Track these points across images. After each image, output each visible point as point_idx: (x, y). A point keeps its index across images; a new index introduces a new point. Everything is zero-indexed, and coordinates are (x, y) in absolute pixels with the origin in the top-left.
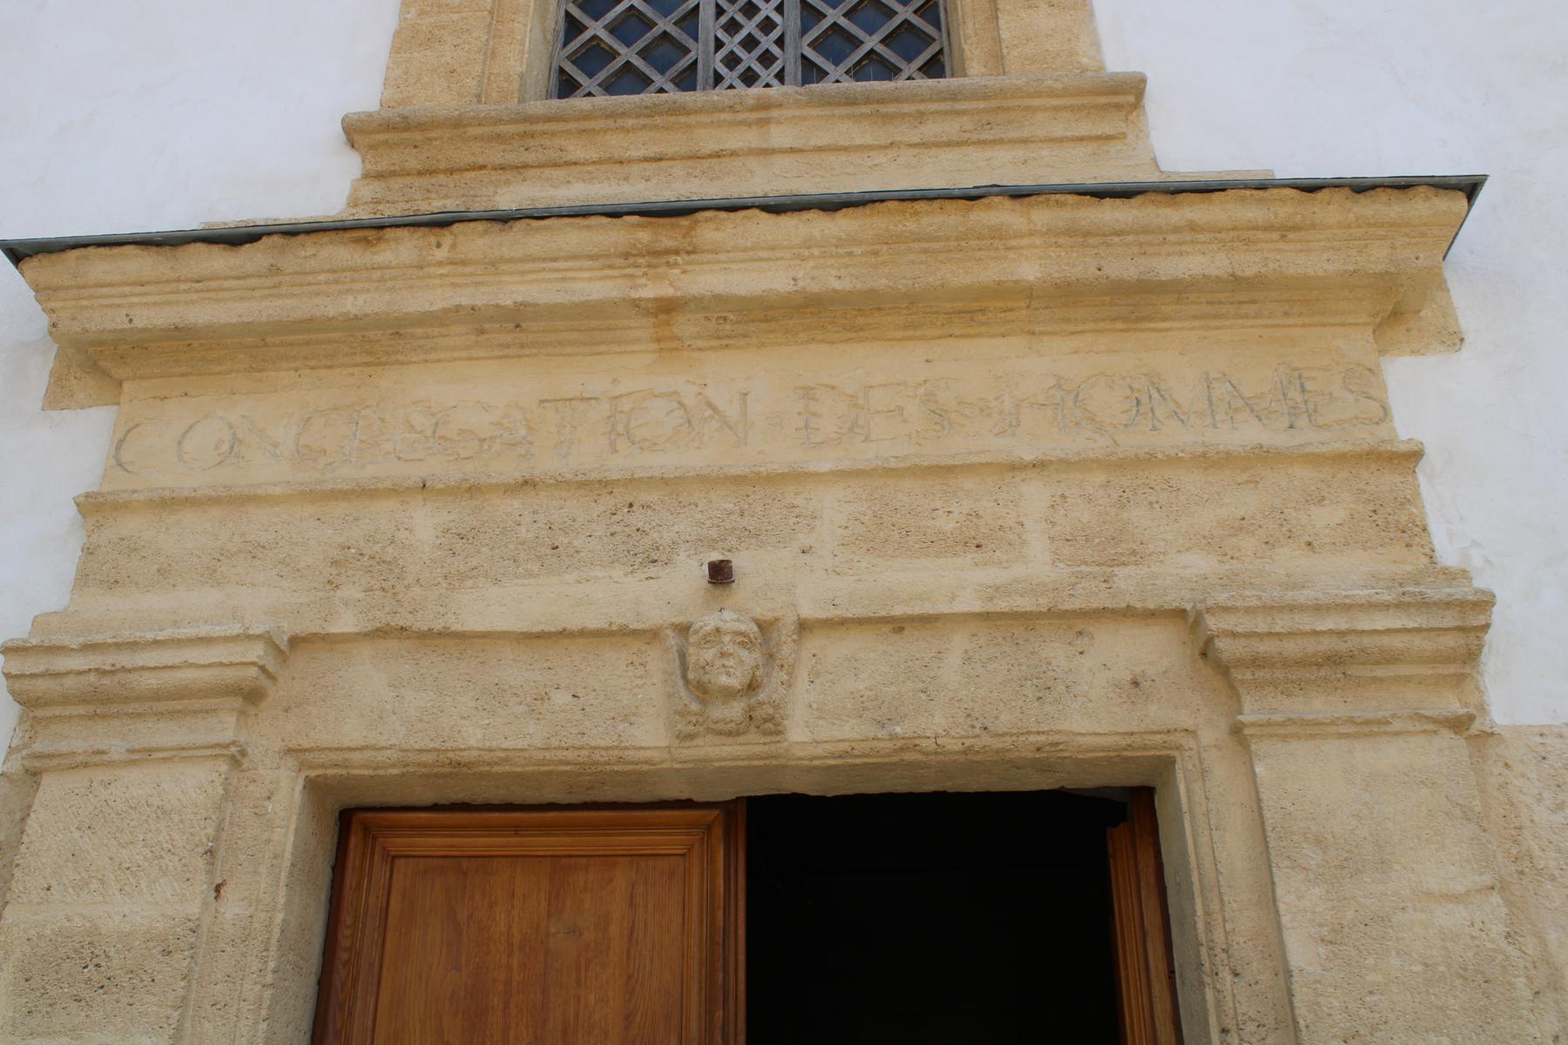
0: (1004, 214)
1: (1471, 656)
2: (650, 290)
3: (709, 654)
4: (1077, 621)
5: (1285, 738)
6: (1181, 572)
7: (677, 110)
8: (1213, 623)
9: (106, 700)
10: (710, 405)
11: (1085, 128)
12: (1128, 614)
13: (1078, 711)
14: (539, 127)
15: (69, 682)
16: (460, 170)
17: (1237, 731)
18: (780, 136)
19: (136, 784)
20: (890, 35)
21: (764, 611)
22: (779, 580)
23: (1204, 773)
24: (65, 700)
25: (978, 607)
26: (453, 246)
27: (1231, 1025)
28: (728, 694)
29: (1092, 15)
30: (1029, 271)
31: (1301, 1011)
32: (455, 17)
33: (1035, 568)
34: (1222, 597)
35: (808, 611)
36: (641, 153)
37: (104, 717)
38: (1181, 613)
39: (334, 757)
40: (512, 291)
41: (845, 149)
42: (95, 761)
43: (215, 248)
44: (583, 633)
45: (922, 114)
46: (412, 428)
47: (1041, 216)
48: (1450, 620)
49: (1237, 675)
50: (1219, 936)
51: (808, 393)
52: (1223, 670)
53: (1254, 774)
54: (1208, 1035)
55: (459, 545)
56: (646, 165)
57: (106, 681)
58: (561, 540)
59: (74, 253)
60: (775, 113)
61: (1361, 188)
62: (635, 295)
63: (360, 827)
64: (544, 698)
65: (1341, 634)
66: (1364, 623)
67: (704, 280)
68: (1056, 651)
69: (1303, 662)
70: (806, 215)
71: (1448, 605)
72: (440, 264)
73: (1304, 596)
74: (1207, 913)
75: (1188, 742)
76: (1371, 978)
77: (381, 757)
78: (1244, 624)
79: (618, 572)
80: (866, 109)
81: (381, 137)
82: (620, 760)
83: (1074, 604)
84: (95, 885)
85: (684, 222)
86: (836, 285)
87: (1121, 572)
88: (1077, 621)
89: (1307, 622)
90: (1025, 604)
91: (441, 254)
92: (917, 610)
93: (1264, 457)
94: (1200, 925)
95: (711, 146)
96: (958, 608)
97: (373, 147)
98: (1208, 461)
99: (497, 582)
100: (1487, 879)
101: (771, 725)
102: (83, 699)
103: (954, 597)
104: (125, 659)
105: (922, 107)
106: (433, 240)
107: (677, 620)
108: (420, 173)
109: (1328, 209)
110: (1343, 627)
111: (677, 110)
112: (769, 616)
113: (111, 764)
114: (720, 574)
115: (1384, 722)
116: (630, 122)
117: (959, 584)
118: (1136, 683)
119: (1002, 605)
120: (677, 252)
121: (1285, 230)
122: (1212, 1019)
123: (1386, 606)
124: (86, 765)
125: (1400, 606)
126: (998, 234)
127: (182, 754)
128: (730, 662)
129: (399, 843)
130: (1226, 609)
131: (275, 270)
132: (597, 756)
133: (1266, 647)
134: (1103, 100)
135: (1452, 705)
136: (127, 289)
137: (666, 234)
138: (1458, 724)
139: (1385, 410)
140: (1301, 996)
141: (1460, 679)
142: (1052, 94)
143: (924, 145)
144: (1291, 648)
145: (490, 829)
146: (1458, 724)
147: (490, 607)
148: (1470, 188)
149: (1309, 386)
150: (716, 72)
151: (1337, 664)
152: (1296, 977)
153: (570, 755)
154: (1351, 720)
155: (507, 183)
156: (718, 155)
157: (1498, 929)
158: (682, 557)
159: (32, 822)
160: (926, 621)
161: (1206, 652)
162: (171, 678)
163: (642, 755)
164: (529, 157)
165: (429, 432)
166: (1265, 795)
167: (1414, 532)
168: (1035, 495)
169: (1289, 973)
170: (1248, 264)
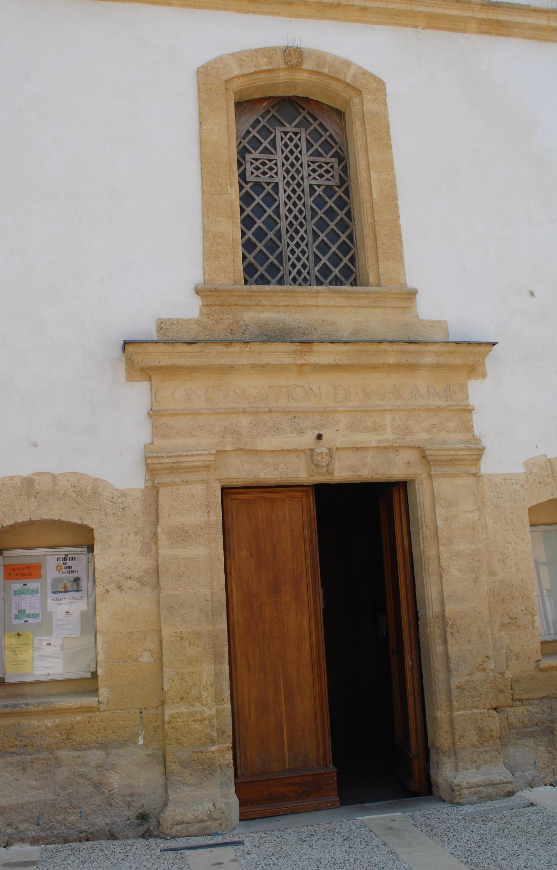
0: (387, 347)
1: (479, 460)
2: (299, 362)
3: (319, 458)
4: (396, 449)
5: (439, 477)
6: (420, 437)
7: (293, 292)
8: (428, 452)
9: (174, 469)
10: (311, 389)
11: (401, 304)
12: (408, 447)
13: (396, 472)
14: (254, 294)
15: (165, 465)
16: (231, 305)
17: (430, 475)
18: (321, 301)
19: (185, 489)
20: (348, 266)
21: (328, 445)
22: (336, 437)
23: (422, 484)
24: (164, 469)
25: (376, 445)
26: (250, 348)
27: (425, 537)
28: (323, 467)
29: (404, 264)
30: (391, 360)
31: (439, 534)
32: (222, 248)
33: (389, 435)
34: (430, 447)
35: (338, 446)
36: (283, 304)
37: (173, 473)
38: (420, 447)
39: (229, 480)
40: (264, 360)
41: (338, 306)
42: (174, 484)
43: (185, 344)
44: (287, 450)
45: (359, 297)
46: (236, 393)
47: (396, 347)
48: (476, 453)
49: (431, 463)
50: (423, 519)
51: (335, 387)
52: (428, 462)
53: (433, 485)
54: (420, 540)
55: (254, 427)
56: (284, 307)
57: (175, 465)
58: (279, 426)
59: (144, 344)
60: (320, 294)
61: (469, 343)
62: (296, 362)
63: (226, 491)
64: (278, 466)
65: (453, 455)
66: (458, 453)
67: (314, 359)
68: (392, 455)
69: (445, 461)
70: (339, 344)
71: (476, 449)
72: (246, 352)
73: (447, 446)
74: (421, 514)
75: (419, 477)
76: (453, 528)
77: (240, 480)
78: (434, 453)
79: (294, 435)
80: (344, 295)
81: (208, 293)
82: (297, 480)
83: (397, 445)
84: (180, 514)
85: (310, 345)
86: (346, 362)
87: (407, 437)
88: (396, 449)
89: (447, 453)
90: (386, 445)
91: (247, 350)
92: (363, 445)
93: (439, 409)
94: (419, 516)
95: (302, 303)
96: (372, 445)
97: (205, 296)
98: (428, 410)
99: (265, 437)
100: (476, 508)
101: (330, 472)
102: (168, 469)
103: (370, 443)
104: (179, 459)
105: (359, 295)
106: (245, 346)
107: (309, 448)
108: (219, 306)
109: (461, 349)
110: (454, 454)
111: (293, 292)
112: (330, 447)
113: (178, 485)
114: (320, 437)
115: (460, 474)
116: (280, 294)
117: (371, 439)
118: (408, 463)
119: (381, 445)
120: (307, 352)
121: (451, 353)
122: (421, 535)
123: (463, 449)
124: (171, 485)
125: (466, 449)
126: (385, 351)
127: (196, 482)
128: (324, 460)
129: (233, 496)
130: (430, 450)
131: (201, 351)
132: (291, 480)
133: (437, 458)
134: (406, 296)
135: (473, 470)
136: (159, 354)
137: (305, 348)
138: (474, 475)
139: (467, 396)
140: (439, 531)
141: (476, 464)
142: (393, 294)
143: (359, 307)
144: (443, 458)
145: (256, 493)
146: (474, 475)
147: (265, 443)
148: (494, 344)
149: (451, 389)
150: (289, 256)
151: (452, 461)
152: (439, 528)
153: (285, 479)
154: (453, 474)
155: (245, 311)
156: (304, 306)
157: (477, 518)
158: (309, 431)
159: (160, 500)
160: (364, 448)
161: (425, 457)
162: (191, 464)
163: (301, 479)
164: (252, 303)
165: (241, 395)
166: (435, 490)
167: (469, 428)
168: (388, 417)
169: (437, 527)
170: (442, 360)
